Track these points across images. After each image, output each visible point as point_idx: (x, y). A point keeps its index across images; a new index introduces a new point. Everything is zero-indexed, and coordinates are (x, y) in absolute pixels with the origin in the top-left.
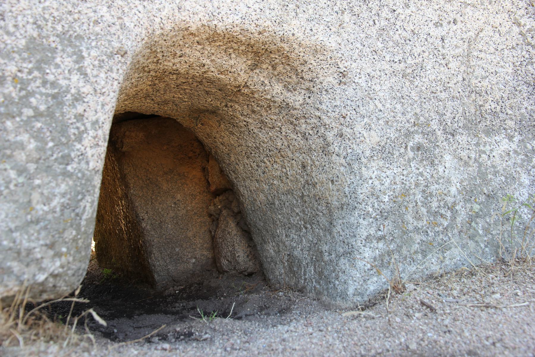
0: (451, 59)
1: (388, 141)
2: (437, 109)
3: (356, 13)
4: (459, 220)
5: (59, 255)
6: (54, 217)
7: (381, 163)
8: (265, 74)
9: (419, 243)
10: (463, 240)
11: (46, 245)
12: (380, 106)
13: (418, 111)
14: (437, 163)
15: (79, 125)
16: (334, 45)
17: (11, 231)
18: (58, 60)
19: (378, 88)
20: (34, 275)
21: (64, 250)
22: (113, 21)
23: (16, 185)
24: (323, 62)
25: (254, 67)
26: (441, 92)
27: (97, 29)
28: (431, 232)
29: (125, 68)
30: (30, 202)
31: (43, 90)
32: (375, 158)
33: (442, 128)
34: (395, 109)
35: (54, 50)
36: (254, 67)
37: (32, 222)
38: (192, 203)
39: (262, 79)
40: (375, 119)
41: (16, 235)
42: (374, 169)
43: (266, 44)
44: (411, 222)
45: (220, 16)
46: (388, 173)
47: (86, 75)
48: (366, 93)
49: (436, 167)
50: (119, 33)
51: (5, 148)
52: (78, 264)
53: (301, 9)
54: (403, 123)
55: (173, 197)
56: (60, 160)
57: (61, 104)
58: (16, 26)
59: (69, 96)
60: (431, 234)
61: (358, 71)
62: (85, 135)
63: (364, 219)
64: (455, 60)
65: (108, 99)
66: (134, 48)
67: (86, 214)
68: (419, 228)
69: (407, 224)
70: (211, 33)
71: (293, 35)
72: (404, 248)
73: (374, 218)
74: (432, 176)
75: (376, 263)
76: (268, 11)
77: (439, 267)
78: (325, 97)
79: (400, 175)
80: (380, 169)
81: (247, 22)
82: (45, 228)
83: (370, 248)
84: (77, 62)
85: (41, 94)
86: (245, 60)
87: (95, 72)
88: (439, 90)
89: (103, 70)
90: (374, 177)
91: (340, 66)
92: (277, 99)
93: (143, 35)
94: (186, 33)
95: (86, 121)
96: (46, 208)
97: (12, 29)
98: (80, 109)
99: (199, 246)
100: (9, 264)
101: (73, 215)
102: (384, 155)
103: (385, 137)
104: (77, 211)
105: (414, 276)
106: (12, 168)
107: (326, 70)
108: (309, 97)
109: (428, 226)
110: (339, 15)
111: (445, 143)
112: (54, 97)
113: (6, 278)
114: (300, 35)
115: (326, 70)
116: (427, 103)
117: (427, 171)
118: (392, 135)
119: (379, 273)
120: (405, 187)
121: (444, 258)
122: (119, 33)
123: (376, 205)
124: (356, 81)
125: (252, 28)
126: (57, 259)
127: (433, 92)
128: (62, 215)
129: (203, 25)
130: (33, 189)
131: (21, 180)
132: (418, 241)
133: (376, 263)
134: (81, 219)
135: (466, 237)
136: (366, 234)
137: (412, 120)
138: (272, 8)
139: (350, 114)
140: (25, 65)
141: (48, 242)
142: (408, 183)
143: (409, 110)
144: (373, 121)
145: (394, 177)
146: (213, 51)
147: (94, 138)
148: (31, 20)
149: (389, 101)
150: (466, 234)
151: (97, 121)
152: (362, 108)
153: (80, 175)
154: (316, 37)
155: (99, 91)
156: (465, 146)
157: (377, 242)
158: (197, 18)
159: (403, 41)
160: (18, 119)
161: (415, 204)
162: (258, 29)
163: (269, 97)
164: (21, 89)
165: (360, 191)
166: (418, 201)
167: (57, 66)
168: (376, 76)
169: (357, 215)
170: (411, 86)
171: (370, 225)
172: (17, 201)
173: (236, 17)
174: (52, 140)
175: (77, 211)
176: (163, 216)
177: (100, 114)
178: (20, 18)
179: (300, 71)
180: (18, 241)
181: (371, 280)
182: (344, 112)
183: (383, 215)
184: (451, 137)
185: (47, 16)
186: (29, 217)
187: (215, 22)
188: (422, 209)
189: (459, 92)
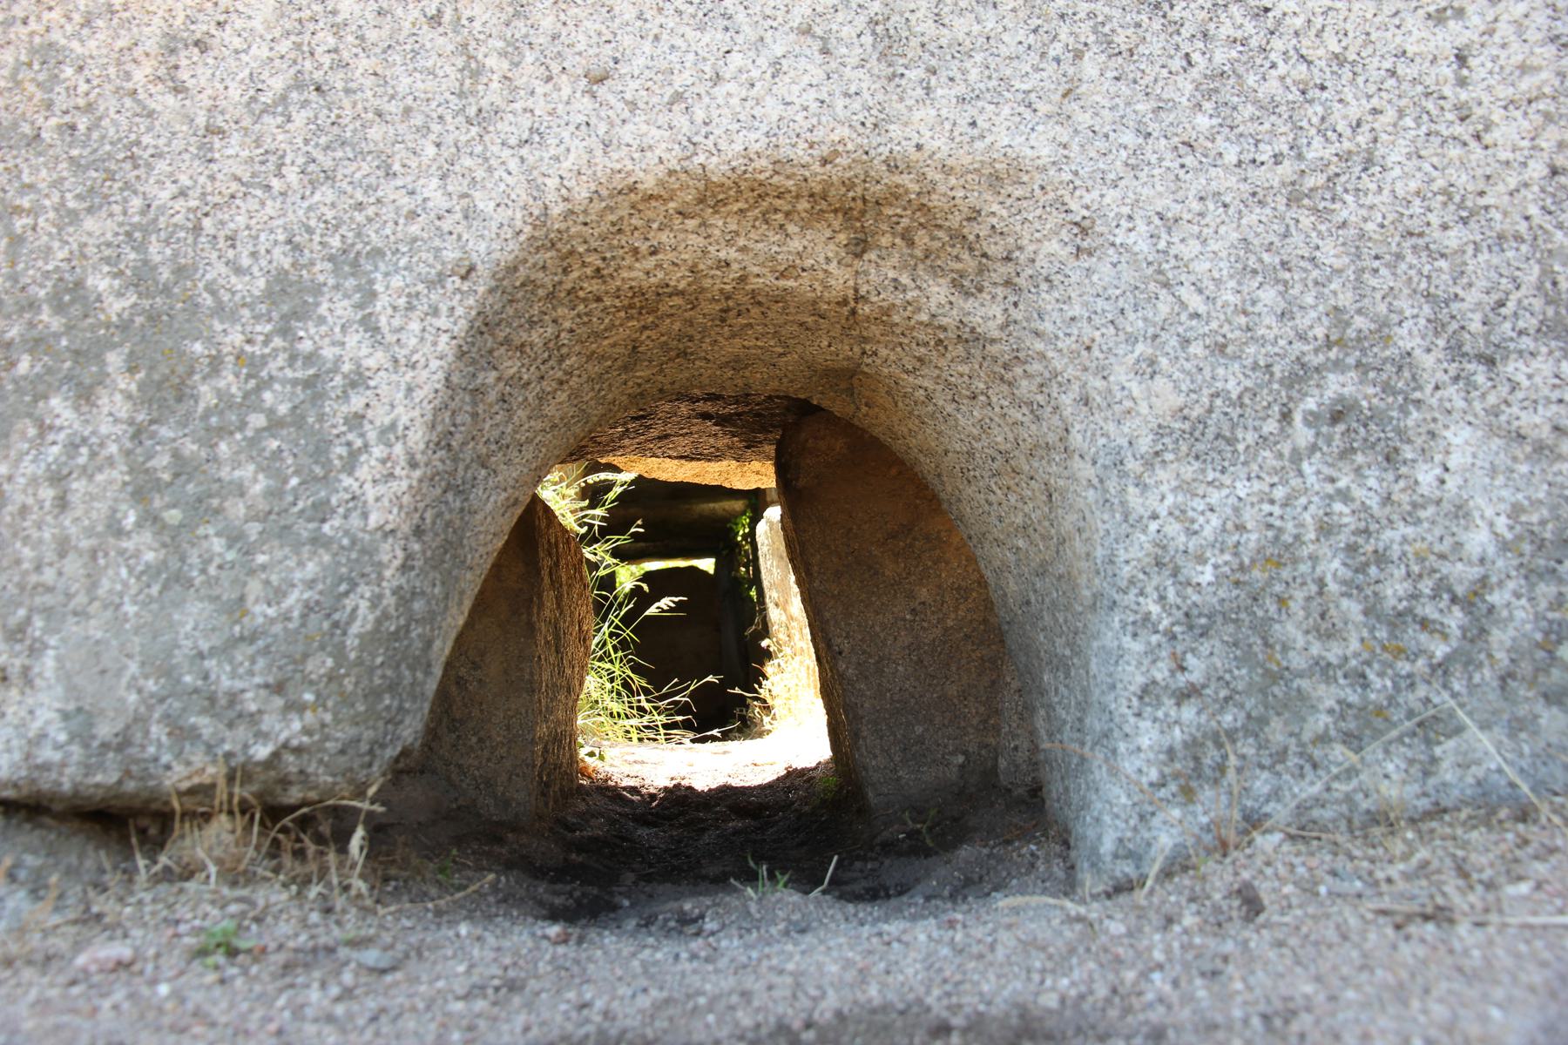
0: (1497, 115)
1: (1218, 402)
2: (1424, 285)
3: (1123, 47)
4: (1500, 638)
5: (299, 708)
6: (285, 629)
7: (1189, 470)
8: (895, 260)
9: (1331, 711)
10: (1515, 703)
11: (267, 686)
12: (1196, 303)
13: (1346, 299)
14: (1409, 456)
15: (350, 437)
16: (1045, 152)
17: (201, 656)
18: (323, 309)
19: (1191, 249)
20: (246, 746)
21: (309, 697)
22: (447, 205)
23: (220, 567)
24: (1025, 204)
25: (860, 247)
26: (1445, 227)
27: (414, 229)
28: (1381, 675)
29: (471, 301)
30: (242, 599)
31: (289, 373)
32: (1169, 456)
33: (1441, 343)
34: (1254, 303)
35: (317, 289)
36: (860, 247)
37: (242, 638)
38: (956, 609)
39: (892, 274)
40: (1174, 342)
41: (211, 664)
42: (1164, 488)
43: (854, 185)
44: (1300, 643)
45: (710, 143)
46: (1215, 497)
47: (377, 329)
48: (1150, 271)
49: (1404, 470)
50: (460, 229)
51: (210, 496)
52: (352, 731)
53: (943, 74)
54: (1282, 342)
55: (911, 596)
56: (308, 513)
57: (318, 397)
58: (254, 254)
59: (338, 380)
60: (1377, 682)
61: (1126, 210)
62: (363, 458)
63: (1135, 635)
64: (1518, 114)
65: (425, 374)
66: (496, 255)
67: (358, 623)
68: (1329, 664)
69: (1285, 648)
70: (701, 185)
71: (919, 147)
72: (1276, 724)
73: (1165, 633)
74: (1387, 500)
75: (1178, 766)
76: (840, 102)
77: (1415, 788)
78: (1047, 299)
79: (1261, 501)
80: (1184, 487)
81: (783, 141)
82: (266, 651)
83: (1155, 720)
84: (359, 306)
85: (284, 382)
86: (828, 233)
87: (396, 322)
88: (1434, 219)
89: (416, 315)
90: (1163, 513)
91: (1073, 206)
92: (944, 321)
93: (519, 224)
94: (632, 201)
95: (367, 427)
96: (271, 612)
97: (245, 261)
98: (357, 402)
99: (975, 722)
100: (192, 720)
101: (326, 625)
102: (1200, 447)
103: (1206, 392)
104: (336, 616)
105: (1316, 813)
106: (218, 534)
107: (1037, 225)
108: (1016, 304)
109: (1365, 656)
110: (1064, 66)
111: (1451, 391)
112: (308, 383)
113: (188, 747)
114: (938, 144)
115: (1037, 225)
116: (1383, 271)
117: (1370, 487)
118: (1231, 385)
119: (1188, 794)
120: (1277, 538)
121: (1434, 760)
122: (460, 229)
123: (1171, 594)
124: (1118, 241)
125: (800, 153)
126: (293, 716)
127: (1411, 234)
128: (303, 625)
129: (671, 173)
130: (252, 572)
131: (231, 556)
132: (1330, 703)
133: (1178, 766)
134: (345, 633)
135: (1530, 694)
136: (1140, 680)
137: (1320, 332)
138: (853, 90)
139: (1104, 336)
140: (258, 328)
141: (271, 680)
142: (1290, 526)
143: (1309, 299)
144: (1168, 349)
145: (1236, 510)
146: (734, 227)
147: (383, 461)
148: (281, 238)
149: (1232, 284)
150: (1532, 683)
151: (393, 426)
152: (1131, 316)
153: (345, 542)
154: (988, 140)
155: (403, 361)
156: (1546, 391)
157: (1178, 704)
158: (651, 158)
159: (1295, 95)
160: (238, 436)
161: (1314, 588)
162: (815, 152)
163: (924, 317)
164: (249, 376)
165: (1122, 555)
166: (1329, 578)
167: (322, 320)
168: (1186, 216)
169: (1117, 625)
170: (1323, 228)
171: (1152, 653)
172: (218, 598)
173: (753, 136)
174: (297, 473)
175: (336, 616)
176: (884, 642)
177: (400, 410)
178: (263, 237)
179: (971, 238)
180: (213, 677)
181: (1160, 816)
182: (1088, 331)
183: (1197, 624)
184: (1482, 368)
185: (313, 223)
186: (237, 629)
187: (701, 159)
188: (1345, 603)
189: (1527, 218)
